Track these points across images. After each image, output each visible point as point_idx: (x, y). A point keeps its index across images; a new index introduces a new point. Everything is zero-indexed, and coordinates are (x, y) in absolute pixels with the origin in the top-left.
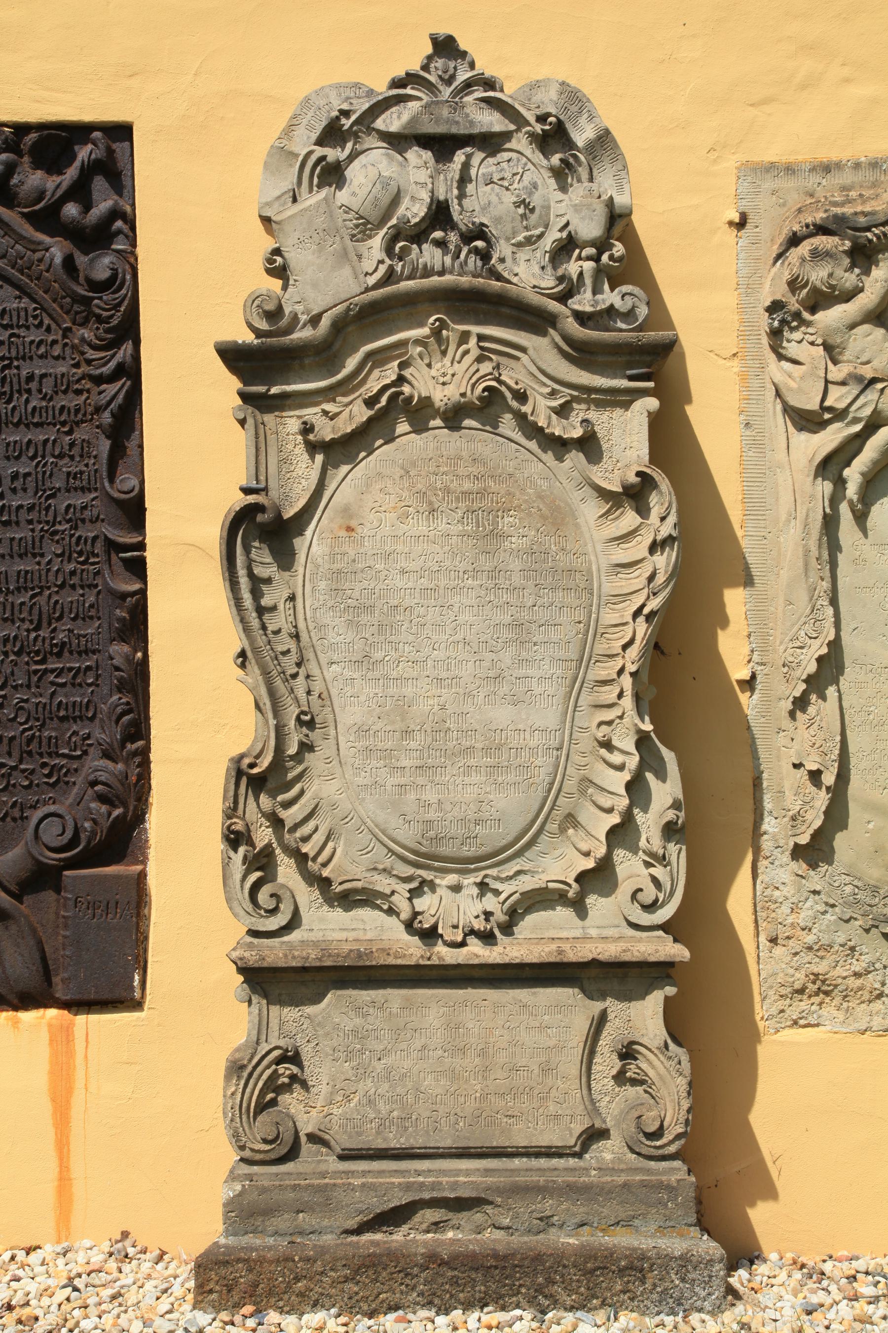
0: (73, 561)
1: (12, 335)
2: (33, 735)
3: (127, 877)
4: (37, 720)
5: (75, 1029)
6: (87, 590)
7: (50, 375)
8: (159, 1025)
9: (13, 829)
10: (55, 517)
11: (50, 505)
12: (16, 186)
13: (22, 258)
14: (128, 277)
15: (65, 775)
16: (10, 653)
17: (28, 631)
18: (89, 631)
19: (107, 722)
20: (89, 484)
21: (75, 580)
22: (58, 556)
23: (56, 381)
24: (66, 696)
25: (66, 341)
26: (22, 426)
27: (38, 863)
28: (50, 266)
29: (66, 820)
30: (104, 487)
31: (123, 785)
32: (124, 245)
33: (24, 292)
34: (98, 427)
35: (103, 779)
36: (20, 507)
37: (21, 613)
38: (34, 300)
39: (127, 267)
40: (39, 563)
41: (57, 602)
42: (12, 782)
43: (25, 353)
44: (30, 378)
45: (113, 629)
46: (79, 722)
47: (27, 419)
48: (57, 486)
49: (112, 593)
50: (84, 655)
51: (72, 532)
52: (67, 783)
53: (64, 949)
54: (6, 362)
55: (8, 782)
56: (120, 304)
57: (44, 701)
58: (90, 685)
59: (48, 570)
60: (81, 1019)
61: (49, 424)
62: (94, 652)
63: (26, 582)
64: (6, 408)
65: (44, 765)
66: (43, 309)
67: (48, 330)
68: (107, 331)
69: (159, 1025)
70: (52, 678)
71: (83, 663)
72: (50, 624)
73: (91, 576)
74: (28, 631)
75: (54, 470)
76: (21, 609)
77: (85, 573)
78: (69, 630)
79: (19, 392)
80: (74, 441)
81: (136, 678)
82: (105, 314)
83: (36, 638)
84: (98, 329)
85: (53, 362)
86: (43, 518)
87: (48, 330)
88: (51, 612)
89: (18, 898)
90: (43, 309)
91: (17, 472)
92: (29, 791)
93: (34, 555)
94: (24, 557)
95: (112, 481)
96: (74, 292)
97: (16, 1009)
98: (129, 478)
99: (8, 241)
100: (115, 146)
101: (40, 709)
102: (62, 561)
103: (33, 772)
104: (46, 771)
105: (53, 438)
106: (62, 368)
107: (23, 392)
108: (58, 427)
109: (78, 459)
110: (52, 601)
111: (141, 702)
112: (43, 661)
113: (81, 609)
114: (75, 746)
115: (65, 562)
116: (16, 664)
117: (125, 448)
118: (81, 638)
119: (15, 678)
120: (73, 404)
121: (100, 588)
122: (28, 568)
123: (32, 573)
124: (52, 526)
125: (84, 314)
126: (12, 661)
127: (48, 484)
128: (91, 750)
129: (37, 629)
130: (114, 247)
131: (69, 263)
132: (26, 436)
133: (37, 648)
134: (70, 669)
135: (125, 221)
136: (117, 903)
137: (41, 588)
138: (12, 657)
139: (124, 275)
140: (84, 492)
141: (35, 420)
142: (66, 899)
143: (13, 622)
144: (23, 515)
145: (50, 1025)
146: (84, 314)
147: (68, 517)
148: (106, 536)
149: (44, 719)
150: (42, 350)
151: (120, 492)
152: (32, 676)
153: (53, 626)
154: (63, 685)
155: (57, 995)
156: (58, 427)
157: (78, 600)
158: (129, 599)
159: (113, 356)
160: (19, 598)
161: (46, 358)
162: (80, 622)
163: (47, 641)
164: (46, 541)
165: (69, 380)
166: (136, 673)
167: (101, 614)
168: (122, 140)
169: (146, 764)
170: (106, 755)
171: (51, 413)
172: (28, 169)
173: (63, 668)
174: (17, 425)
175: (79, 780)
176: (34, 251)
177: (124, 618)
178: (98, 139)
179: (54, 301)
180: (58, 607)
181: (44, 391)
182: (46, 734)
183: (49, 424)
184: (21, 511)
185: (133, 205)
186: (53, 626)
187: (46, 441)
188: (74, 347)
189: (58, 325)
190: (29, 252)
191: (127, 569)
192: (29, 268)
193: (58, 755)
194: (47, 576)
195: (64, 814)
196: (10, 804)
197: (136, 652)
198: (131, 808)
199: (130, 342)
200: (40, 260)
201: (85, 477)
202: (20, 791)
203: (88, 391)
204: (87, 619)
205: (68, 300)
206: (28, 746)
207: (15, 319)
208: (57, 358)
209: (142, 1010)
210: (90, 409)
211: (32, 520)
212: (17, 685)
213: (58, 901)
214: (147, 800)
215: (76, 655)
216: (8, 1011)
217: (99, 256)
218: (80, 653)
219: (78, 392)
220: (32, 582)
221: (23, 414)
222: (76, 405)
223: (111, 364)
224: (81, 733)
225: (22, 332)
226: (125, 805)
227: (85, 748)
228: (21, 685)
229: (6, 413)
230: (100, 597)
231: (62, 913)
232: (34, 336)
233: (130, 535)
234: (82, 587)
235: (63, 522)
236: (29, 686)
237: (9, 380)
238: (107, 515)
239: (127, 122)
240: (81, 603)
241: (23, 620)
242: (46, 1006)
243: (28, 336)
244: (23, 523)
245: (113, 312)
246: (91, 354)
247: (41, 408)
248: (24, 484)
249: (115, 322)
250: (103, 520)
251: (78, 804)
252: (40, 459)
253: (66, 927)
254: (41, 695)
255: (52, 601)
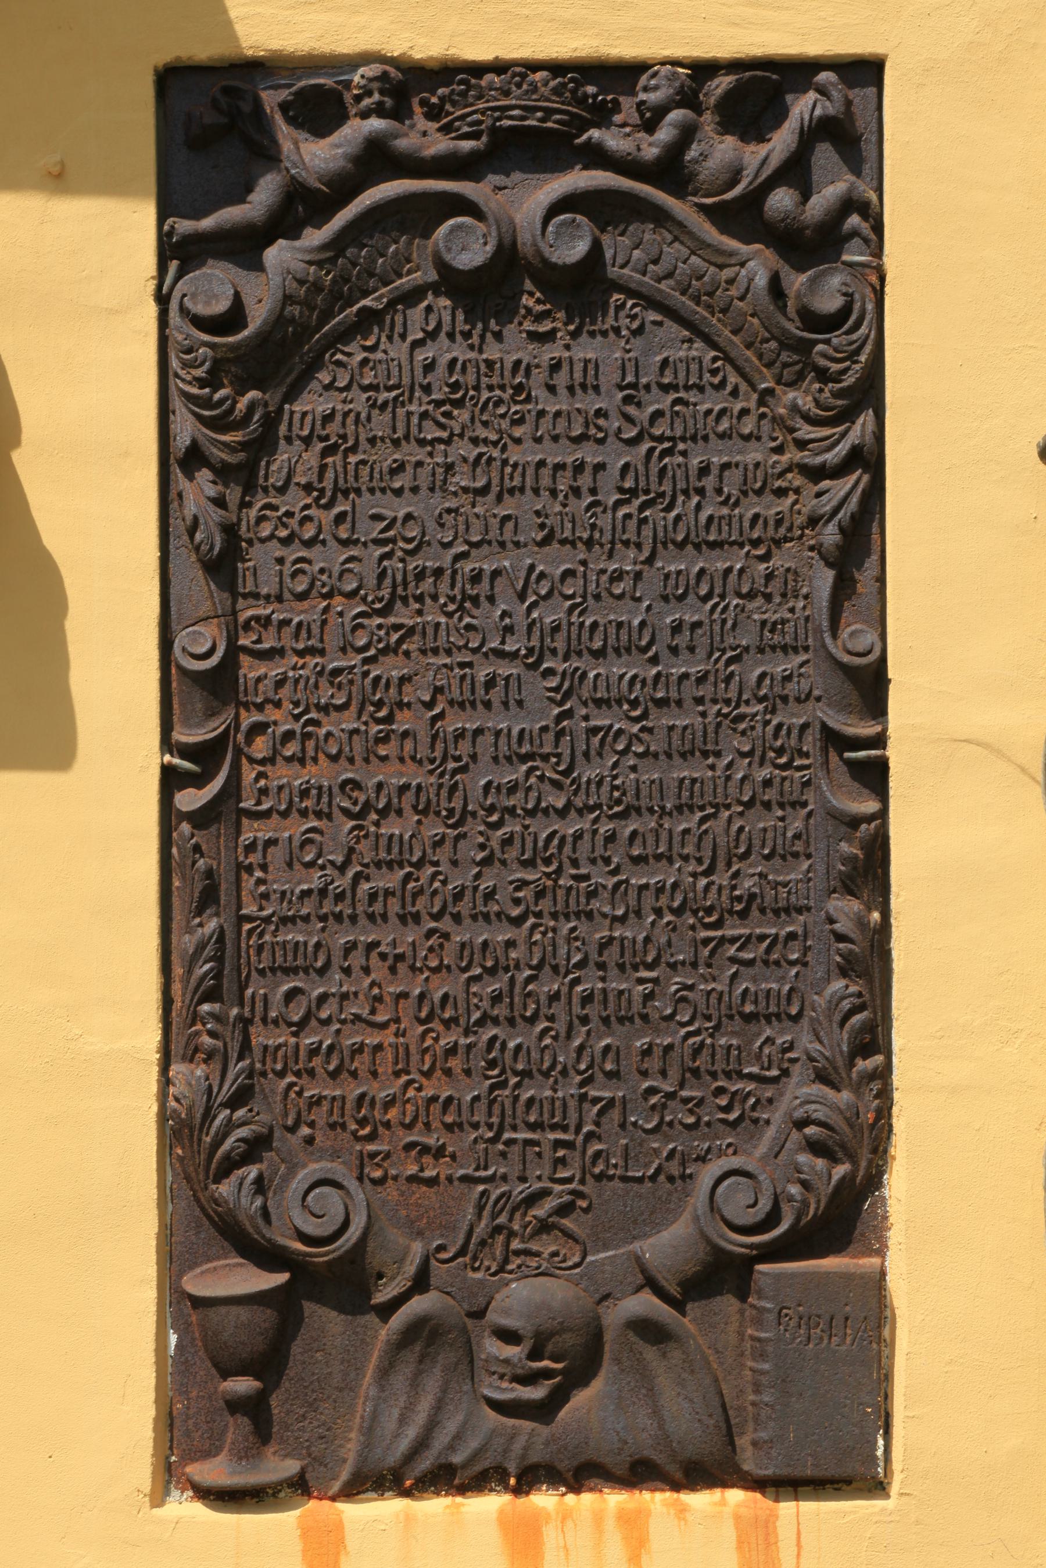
0: (768, 763)
1: (677, 401)
2: (702, 1044)
3: (862, 1276)
4: (708, 1018)
5: (778, 1524)
6: (789, 809)
7: (737, 465)
8: (918, 1522)
9: (670, 1194)
10: (740, 694)
11: (732, 674)
12: (695, 161)
13: (700, 278)
14: (870, 307)
15: (753, 1108)
16: (666, 911)
17: (694, 875)
18: (792, 876)
19: (825, 1024)
20: (796, 639)
21: (770, 795)
22: (743, 755)
23: (745, 475)
24: (754, 980)
25: (762, 410)
26: (689, 547)
27: (717, 1251)
28: (747, 290)
29: (758, 1182)
30: (824, 646)
31: (851, 1126)
32: (861, 254)
33: (697, 331)
34: (812, 548)
35: (819, 1115)
36: (685, 676)
37: (683, 846)
38: (713, 345)
39: (868, 291)
40: (712, 768)
41: (741, 829)
42: (668, 1119)
43: (697, 430)
44: (704, 470)
45: (834, 874)
46: (775, 1023)
47: (697, 536)
48: (744, 643)
49: (836, 816)
50: (783, 915)
51: (768, 717)
52: (756, 1121)
53: (757, 1391)
54: (666, 445)
55: (662, 1118)
56: (858, 352)
57: (719, 988)
58: (793, 963)
59: (728, 778)
60: (787, 1508)
61: (732, 544)
62: (799, 911)
63: (692, 797)
64: (665, 518)
65: (720, 1091)
66: (728, 359)
67: (735, 393)
68: (835, 395)
69: (918, 1522)
70: (732, 951)
71: (782, 928)
72: (729, 865)
73: (797, 787)
74: (694, 875)
75: (741, 617)
76: (683, 839)
77: (787, 784)
78: (761, 875)
79: (686, 492)
80: (773, 571)
81: (872, 952)
82: (835, 367)
83: (707, 888)
84: (821, 390)
85: (741, 443)
86: (721, 694)
87: (735, 393)
88: (732, 845)
89: (679, 1305)
90: (728, 359)
91: (681, 621)
92: (693, 1133)
93: (705, 754)
94: (689, 757)
95: (835, 636)
96: (785, 331)
97: (676, 1487)
98: (862, 631)
99: (679, 251)
100: (851, 94)
101: (713, 1000)
102: (750, 764)
103: (701, 1102)
104: (723, 1102)
105: (738, 566)
106: (754, 455)
107: (692, 492)
108: (747, 549)
109: (777, 599)
110: (735, 827)
111: (878, 991)
112: (718, 925)
113: (780, 841)
114: (770, 1061)
115: (755, 765)
116: (674, 929)
117: (854, 581)
118: (780, 888)
119: (673, 950)
120: (773, 511)
121: (810, 808)
122: (696, 775)
123: (702, 783)
124: (735, 708)
125: (798, 367)
126: (669, 923)
127: (730, 641)
128: (796, 1069)
129: (709, 872)
130: (846, 257)
131: (776, 289)
132: (693, 563)
133: (709, 903)
134: (762, 938)
135: (865, 216)
136: (847, 1319)
137: (716, 806)
138: (668, 918)
139: (864, 304)
140: (786, 653)
141: (711, 538)
142: (762, 1310)
143: (670, 860)
144: (689, 690)
145: (737, 1518)
146: (798, 367)
147: (762, 693)
148: (824, 725)
149: (720, 1017)
150: (724, 425)
151: (850, 653)
152: (700, 947)
153: (734, 868)
154: (751, 963)
155: (746, 1467)
156: (747, 549)
157: (775, 826)
158: (864, 826)
159: (843, 435)
160: (680, 823)
161: (730, 437)
162: (777, 861)
163: (725, 893)
164: (725, 731)
165: (766, 474)
166: (872, 946)
167: (812, 849)
168: (863, 85)
169: (885, 1095)
170: (822, 1077)
171: (735, 525)
172: (712, 134)
173: (750, 935)
174: (681, 545)
175: (777, 1116)
176: (721, 267)
177: (856, 856)
178: (832, 84)
179: (749, 346)
180: (743, 837)
181: (726, 490)
182: (723, 1041)
183: (732, 544)
184: (686, 683)
185: (880, 190)
186: (734, 868)
187: (729, 571)
188: (777, 421)
189: (753, 386)
190: (712, 269)
191: (854, 777)
192: (711, 294)
193: (741, 1076)
194: (726, 787)
195: (756, 1172)
196: (665, 1154)
197: (870, 910)
198: (863, 1164)
199: (871, 411)
200: (731, 282)
201: (789, 628)
202: (681, 1132)
203: (797, 491)
204: (789, 858)
205: (773, 345)
206: (694, 1060)
207: (682, 375)
208: (747, 438)
209: (887, 1496)
210: (799, 520)
211: (703, 697)
212: (676, 963)
213: (742, 1312)
214: (885, 1151)
215: (770, 915)
216: (663, 1490)
217: (823, 274)
218: (777, 912)
219: (781, 492)
220: (702, 796)
221: (693, 528)
222: (778, 513)
223: (840, 446)
224: (779, 1041)
225: (692, 397)
226: (853, 1159)
227: (786, 1065)
228: (683, 963)
229: (665, 526)
230: (812, 821)
231: (749, 1331)
232: (712, 402)
233: (862, 723)
234: (782, 806)
235: (753, 702)
236: (694, 965)
237: (670, 474)
238: (825, 691)
239: (876, 55)
240: (780, 831)
241: (686, 858)
242: (725, 1485)
243: (702, 403)
244: (688, 703)
245: (848, 363)
246: (806, 431)
247: (721, 518)
248: (691, 640)
249: (849, 380)
250: (818, 699)
251: (776, 1157)
252: (716, 600)
253: (762, 1356)
254: (714, 980)
255: (735, 827)
